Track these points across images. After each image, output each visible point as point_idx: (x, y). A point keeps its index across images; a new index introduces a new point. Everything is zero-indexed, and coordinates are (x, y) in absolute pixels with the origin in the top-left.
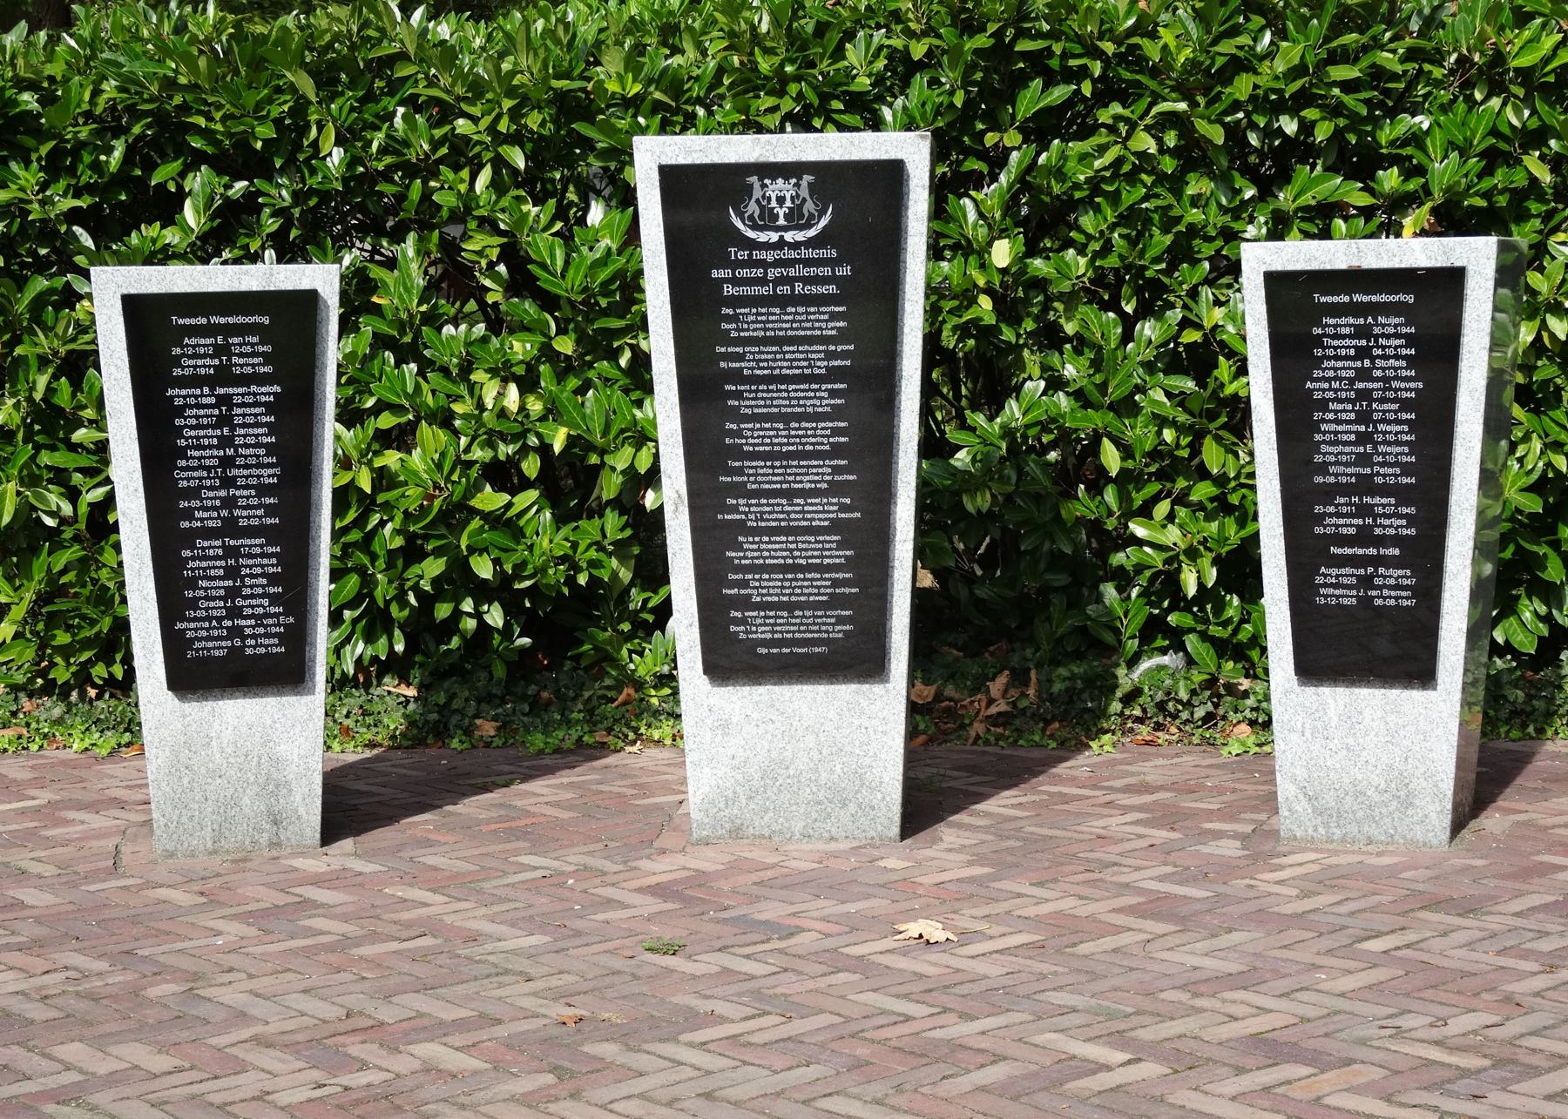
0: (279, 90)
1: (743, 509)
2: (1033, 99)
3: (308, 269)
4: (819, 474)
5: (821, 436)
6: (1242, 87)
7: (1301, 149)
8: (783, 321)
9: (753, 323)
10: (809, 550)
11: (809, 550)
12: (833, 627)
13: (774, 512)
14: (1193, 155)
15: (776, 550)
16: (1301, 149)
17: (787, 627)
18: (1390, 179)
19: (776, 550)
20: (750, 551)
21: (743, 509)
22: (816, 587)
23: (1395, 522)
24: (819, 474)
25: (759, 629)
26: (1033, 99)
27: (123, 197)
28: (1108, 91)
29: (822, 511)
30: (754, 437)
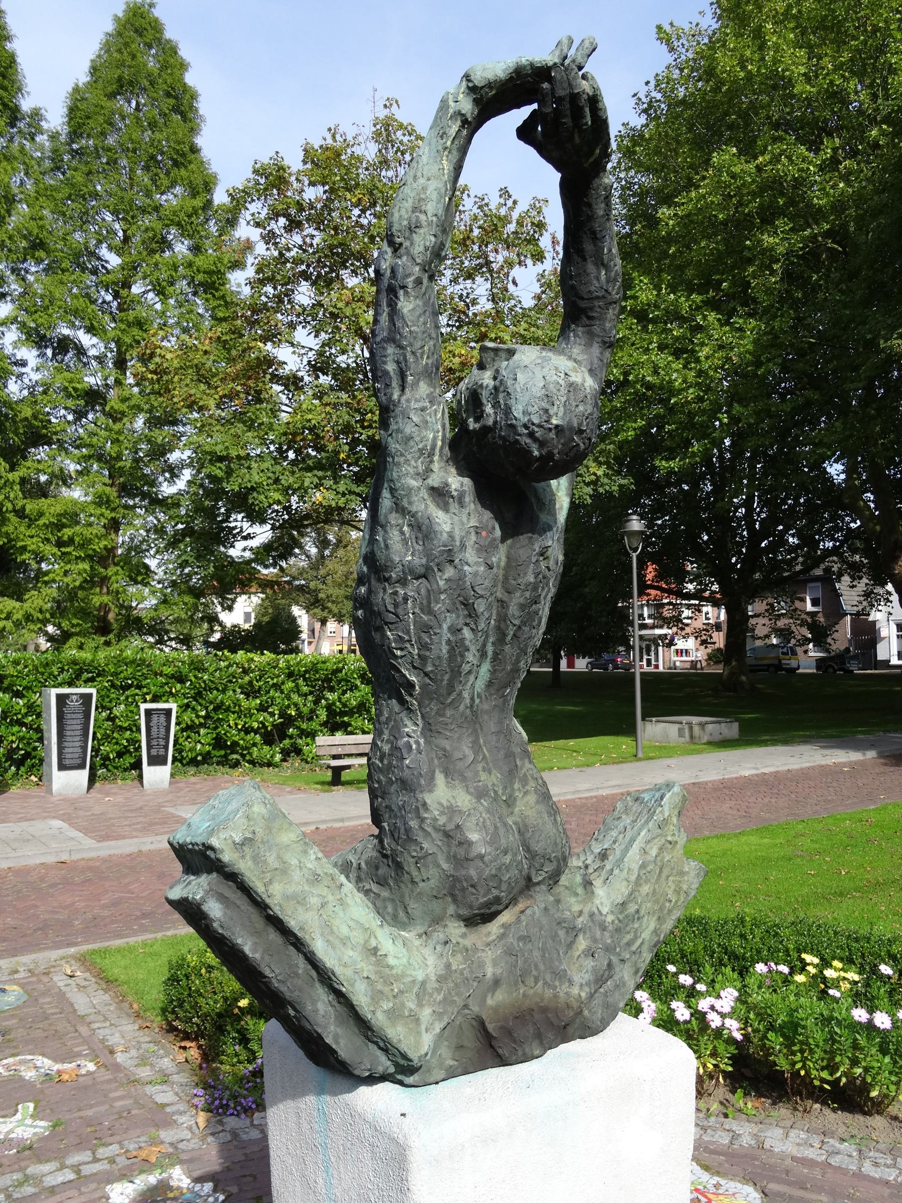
0: (26, 1178)
1: (66, 744)
2: (85, 676)
3: (104, 853)
4: (78, 738)
5: (78, 733)
6: (122, 675)
7: (130, 686)
8: (74, 716)
9: (69, 716)
10: (76, 750)
11: (76, 750)
12: (79, 761)
13: (71, 744)
14: (113, 686)
15: (70, 750)
16: (130, 686)
17: (72, 762)
18: (145, 690)
19: (70, 750)
20: (66, 750)
21: (66, 744)
22: (77, 755)
23: (162, 742)
24: (78, 738)
25: (67, 762)
26: (85, 676)
27: (757, 576)
28: (99, 675)
29: (78, 744)
30: (68, 733)
